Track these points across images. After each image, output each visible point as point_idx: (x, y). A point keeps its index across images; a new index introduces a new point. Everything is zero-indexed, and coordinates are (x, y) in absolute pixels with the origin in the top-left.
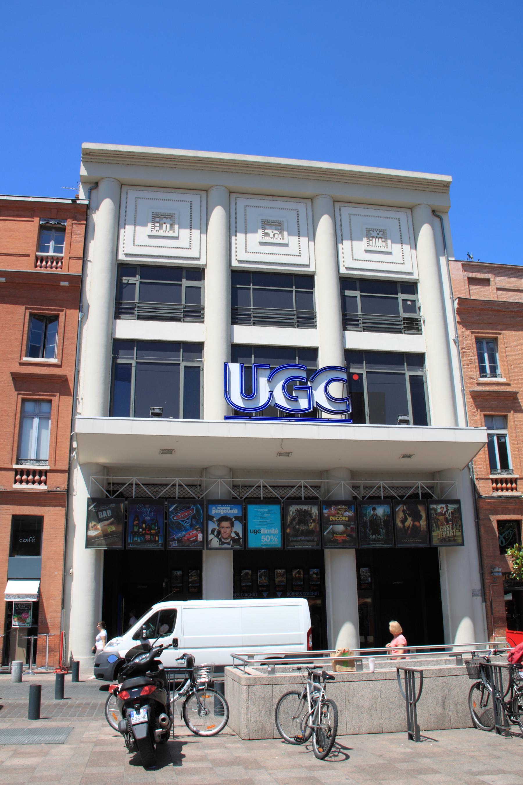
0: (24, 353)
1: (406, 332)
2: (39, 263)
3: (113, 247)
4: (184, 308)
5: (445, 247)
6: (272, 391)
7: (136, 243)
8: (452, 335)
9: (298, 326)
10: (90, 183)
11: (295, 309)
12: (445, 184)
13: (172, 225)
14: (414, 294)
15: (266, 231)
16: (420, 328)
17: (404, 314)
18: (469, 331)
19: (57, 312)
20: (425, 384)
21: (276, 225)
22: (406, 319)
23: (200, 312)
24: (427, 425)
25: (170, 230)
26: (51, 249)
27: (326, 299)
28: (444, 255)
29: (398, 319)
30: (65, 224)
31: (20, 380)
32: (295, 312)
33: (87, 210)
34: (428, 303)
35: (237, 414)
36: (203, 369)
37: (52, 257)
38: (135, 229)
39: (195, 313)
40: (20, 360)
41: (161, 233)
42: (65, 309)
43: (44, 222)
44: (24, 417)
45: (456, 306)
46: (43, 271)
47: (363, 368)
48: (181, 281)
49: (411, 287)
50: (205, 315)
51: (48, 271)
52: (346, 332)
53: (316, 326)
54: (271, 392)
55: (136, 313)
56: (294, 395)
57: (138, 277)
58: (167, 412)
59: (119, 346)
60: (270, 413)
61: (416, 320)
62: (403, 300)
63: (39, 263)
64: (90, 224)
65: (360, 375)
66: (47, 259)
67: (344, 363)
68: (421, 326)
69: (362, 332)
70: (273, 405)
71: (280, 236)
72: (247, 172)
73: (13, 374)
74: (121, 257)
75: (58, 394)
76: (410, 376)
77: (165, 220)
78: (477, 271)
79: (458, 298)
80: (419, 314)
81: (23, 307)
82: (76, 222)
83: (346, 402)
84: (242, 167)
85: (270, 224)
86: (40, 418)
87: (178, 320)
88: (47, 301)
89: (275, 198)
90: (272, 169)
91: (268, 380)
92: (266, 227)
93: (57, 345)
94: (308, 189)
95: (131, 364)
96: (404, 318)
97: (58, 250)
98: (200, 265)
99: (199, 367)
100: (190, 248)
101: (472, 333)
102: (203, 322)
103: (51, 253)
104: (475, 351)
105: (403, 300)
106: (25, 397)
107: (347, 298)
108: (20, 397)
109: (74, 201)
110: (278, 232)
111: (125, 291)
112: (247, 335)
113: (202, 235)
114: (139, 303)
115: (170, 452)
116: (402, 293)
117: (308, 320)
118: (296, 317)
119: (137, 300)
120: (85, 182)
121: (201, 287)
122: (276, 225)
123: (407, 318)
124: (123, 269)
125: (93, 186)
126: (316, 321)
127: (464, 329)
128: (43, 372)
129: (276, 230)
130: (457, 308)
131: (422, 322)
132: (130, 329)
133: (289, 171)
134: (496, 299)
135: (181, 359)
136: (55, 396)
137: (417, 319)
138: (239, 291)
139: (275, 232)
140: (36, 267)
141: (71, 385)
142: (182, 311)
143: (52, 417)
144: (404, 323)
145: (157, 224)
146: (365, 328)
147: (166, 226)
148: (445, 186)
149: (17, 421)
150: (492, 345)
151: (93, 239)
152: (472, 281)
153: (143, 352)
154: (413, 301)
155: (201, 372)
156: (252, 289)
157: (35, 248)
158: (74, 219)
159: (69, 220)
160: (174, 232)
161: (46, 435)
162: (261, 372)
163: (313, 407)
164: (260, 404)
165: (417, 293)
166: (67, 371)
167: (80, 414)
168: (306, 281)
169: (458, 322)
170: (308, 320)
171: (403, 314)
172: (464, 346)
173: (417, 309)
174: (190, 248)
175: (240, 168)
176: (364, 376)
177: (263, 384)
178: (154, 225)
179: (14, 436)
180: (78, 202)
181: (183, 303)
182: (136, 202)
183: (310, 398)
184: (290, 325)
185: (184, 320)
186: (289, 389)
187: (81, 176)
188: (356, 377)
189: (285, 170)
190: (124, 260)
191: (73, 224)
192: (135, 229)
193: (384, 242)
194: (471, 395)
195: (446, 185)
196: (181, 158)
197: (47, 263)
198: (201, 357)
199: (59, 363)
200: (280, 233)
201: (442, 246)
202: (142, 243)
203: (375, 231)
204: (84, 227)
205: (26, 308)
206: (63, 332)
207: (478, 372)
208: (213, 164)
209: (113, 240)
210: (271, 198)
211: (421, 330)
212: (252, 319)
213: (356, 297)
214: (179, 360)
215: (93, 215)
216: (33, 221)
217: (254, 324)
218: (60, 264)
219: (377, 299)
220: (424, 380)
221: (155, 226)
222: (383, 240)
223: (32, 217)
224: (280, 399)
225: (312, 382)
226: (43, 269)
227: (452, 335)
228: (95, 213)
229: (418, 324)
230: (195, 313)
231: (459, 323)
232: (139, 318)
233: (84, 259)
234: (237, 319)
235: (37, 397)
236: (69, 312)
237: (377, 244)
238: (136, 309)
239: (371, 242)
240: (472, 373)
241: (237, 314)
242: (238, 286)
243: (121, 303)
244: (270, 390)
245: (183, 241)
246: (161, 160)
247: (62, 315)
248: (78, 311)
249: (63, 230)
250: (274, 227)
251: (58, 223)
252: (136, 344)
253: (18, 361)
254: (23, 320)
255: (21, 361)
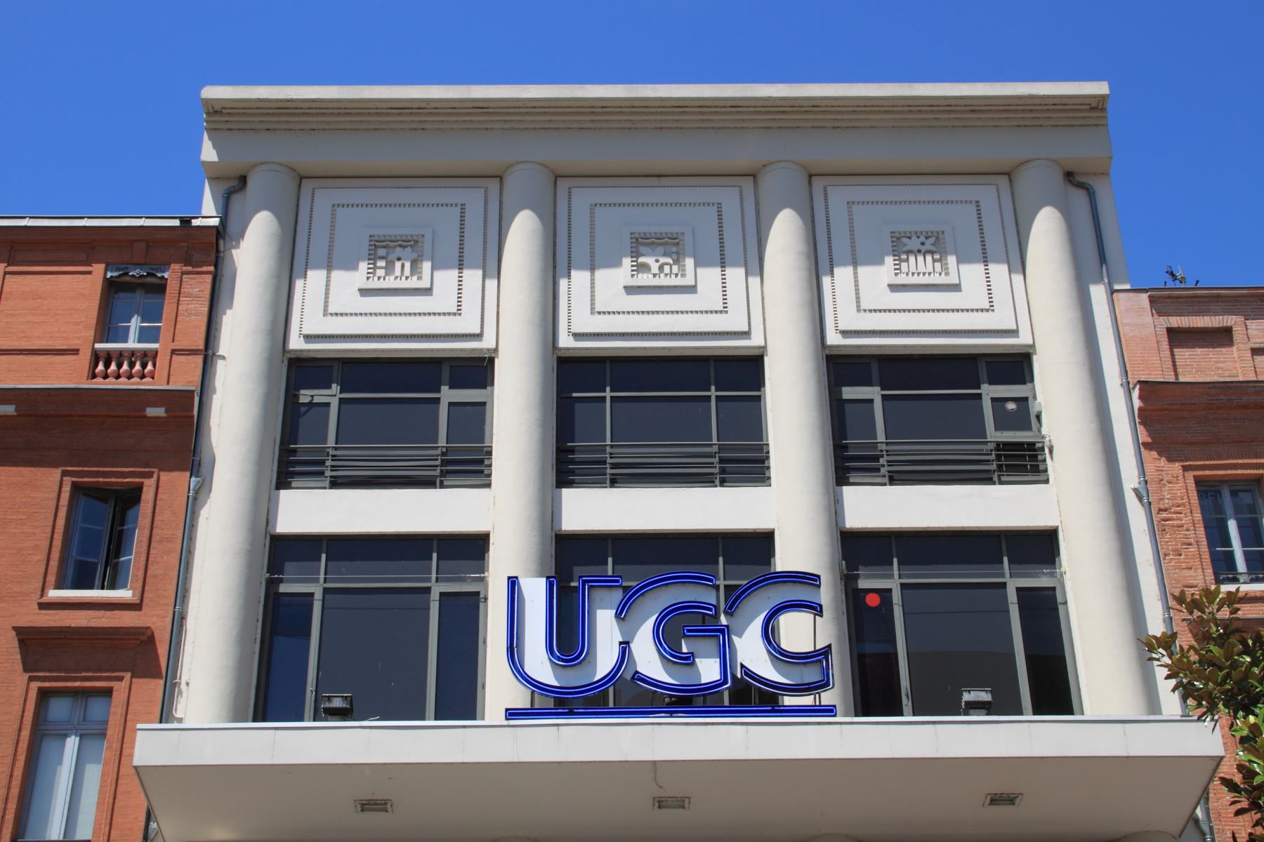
0: (52, 578)
1: (1003, 479)
2: (101, 367)
3: (274, 323)
4: (443, 454)
5: (1103, 259)
6: (627, 643)
7: (331, 310)
8: (1130, 477)
9: (723, 483)
10: (228, 179)
11: (715, 442)
12: (1094, 105)
13: (415, 265)
14: (1024, 383)
15: (641, 260)
16: (1041, 467)
17: (999, 434)
18: (1177, 465)
19: (137, 480)
20: (1061, 608)
21: (666, 244)
22: (1002, 447)
23: (481, 462)
24: (1071, 712)
25: (412, 274)
26: (133, 333)
27: (790, 413)
28: (1102, 279)
29: (984, 447)
30: (166, 275)
31: (37, 646)
32: (715, 449)
33: (217, 240)
34: (1058, 398)
35: (564, 703)
36: (486, 599)
37: (133, 353)
38: (328, 277)
39: (470, 465)
40: (42, 596)
41: (390, 283)
42: (156, 470)
43: (115, 274)
44: (40, 737)
45: (1137, 403)
46: (111, 384)
47: (891, 576)
48: (439, 391)
49: (1016, 366)
50: (493, 468)
51: (109, 383)
52: (846, 489)
53: (769, 478)
54: (625, 646)
55: (328, 473)
56: (685, 650)
57: (335, 388)
58: (402, 706)
59: (284, 552)
60: (625, 696)
61: (1031, 446)
62: (993, 400)
63: (101, 367)
64: (226, 272)
65: (885, 594)
66: (120, 356)
67: (840, 565)
68: (1045, 460)
69: (888, 487)
70: (628, 676)
71: (675, 269)
72: (592, 125)
73: (19, 631)
74: (296, 343)
75: (128, 675)
76: (1018, 589)
77: (399, 251)
78: (1191, 310)
79: (1139, 382)
80: (1039, 431)
81: (57, 472)
82: (190, 268)
83: (820, 661)
84: (580, 113)
85: (653, 243)
86: (81, 736)
87: (428, 483)
88: (111, 456)
89: (664, 181)
90: (651, 113)
91: (618, 616)
92: (642, 249)
93: (133, 558)
94: (742, 153)
95: (312, 595)
96: (998, 444)
97: (144, 335)
98: (481, 350)
99: (478, 593)
100: (724, 311)
101: (1185, 469)
102: (489, 485)
103: (132, 344)
104: (1198, 516)
105: (993, 400)
106: (47, 684)
107: (847, 406)
108: (35, 685)
109: (186, 222)
110: (670, 261)
111: (304, 423)
112: (593, 509)
113: (488, 282)
114: (336, 449)
115: (681, 803)
116: (991, 383)
117: (748, 465)
118: (717, 460)
119: (331, 442)
120: (216, 175)
121: (484, 404)
122: (666, 244)
123: (1005, 444)
124: (299, 372)
125: (233, 186)
126: (768, 468)
127: (1163, 462)
128: (95, 623)
129: (665, 255)
130: (1140, 409)
131: (1047, 451)
132: (311, 510)
133: (694, 113)
134: (1252, 377)
135: (434, 576)
136: (121, 679)
137: (1033, 444)
138: (578, 406)
139: (663, 260)
140: (94, 376)
141: (162, 650)
142: (438, 463)
143: (109, 732)
144: (998, 457)
145: (382, 263)
146: (896, 476)
147: (403, 266)
148: (1093, 109)
149: (21, 745)
150: (1246, 498)
151: (231, 307)
152: (1178, 337)
153: (342, 563)
154: (1023, 401)
155: (482, 605)
156: (608, 400)
157: (91, 333)
158: (187, 262)
159: (173, 266)
160: (420, 278)
161: (93, 775)
162: (599, 594)
163: (734, 676)
164: (598, 676)
165: (1032, 380)
166: (155, 619)
167: (180, 720)
168: (745, 371)
169: (1144, 444)
170: (748, 465)
171: (994, 435)
172: (1166, 503)
173: (1033, 419)
174: (458, 313)
175: (576, 118)
176: (896, 597)
177: (605, 628)
178: (374, 264)
179: (10, 783)
180: (195, 222)
181: (442, 442)
182: (333, 214)
183: (726, 656)
184: (704, 480)
185: (441, 482)
186: (669, 637)
187: (204, 163)
188: (873, 600)
189: (684, 113)
190: (302, 351)
191: (183, 273)
192: (328, 277)
193: (940, 260)
194: (1191, 631)
195: (1096, 105)
196: (432, 105)
197: (120, 366)
198: (482, 568)
199: (136, 600)
200: (676, 262)
201: (1092, 257)
202: (345, 308)
203: (914, 238)
204: (209, 278)
205: (64, 474)
206: (148, 525)
207: (1209, 571)
208: (509, 114)
209: (274, 305)
210: (654, 181)
211: (1046, 471)
212: (609, 471)
213: (871, 401)
214: (429, 580)
215: (234, 251)
216: (90, 273)
217: (614, 483)
218: (150, 367)
219: (926, 403)
220: (1059, 599)
221: (375, 268)
222: (937, 256)
223: (88, 263)
224: (649, 662)
225: (730, 612)
226: (111, 380)
227: (1130, 477)
228: (237, 246)
229: (1036, 456)
230: (470, 465)
231: (1146, 445)
232: (336, 484)
233: (208, 354)
234: (572, 472)
235: (77, 684)
236: (165, 477)
237: (921, 267)
238: (328, 463)
239: (904, 265)
240: (1192, 573)
241: (573, 462)
242: (575, 395)
243: (294, 451)
244: (622, 639)
245: (444, 296)
246: (388, 114)
247: (149, 485)
248: (188, 474)
249: (160, 288)
250: (661, 249)
251: (149, 275)
252: (325, 544)
253: (35, 598)
254: (54, 502)
255: (44, 600)
